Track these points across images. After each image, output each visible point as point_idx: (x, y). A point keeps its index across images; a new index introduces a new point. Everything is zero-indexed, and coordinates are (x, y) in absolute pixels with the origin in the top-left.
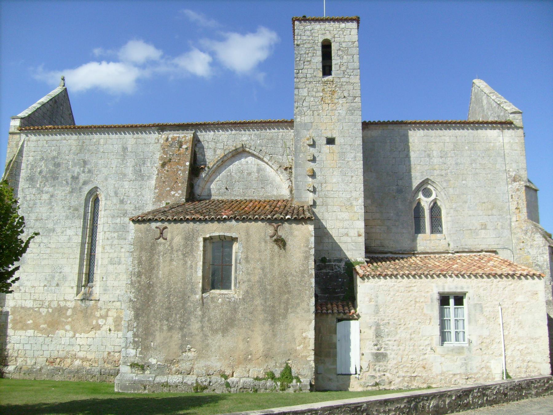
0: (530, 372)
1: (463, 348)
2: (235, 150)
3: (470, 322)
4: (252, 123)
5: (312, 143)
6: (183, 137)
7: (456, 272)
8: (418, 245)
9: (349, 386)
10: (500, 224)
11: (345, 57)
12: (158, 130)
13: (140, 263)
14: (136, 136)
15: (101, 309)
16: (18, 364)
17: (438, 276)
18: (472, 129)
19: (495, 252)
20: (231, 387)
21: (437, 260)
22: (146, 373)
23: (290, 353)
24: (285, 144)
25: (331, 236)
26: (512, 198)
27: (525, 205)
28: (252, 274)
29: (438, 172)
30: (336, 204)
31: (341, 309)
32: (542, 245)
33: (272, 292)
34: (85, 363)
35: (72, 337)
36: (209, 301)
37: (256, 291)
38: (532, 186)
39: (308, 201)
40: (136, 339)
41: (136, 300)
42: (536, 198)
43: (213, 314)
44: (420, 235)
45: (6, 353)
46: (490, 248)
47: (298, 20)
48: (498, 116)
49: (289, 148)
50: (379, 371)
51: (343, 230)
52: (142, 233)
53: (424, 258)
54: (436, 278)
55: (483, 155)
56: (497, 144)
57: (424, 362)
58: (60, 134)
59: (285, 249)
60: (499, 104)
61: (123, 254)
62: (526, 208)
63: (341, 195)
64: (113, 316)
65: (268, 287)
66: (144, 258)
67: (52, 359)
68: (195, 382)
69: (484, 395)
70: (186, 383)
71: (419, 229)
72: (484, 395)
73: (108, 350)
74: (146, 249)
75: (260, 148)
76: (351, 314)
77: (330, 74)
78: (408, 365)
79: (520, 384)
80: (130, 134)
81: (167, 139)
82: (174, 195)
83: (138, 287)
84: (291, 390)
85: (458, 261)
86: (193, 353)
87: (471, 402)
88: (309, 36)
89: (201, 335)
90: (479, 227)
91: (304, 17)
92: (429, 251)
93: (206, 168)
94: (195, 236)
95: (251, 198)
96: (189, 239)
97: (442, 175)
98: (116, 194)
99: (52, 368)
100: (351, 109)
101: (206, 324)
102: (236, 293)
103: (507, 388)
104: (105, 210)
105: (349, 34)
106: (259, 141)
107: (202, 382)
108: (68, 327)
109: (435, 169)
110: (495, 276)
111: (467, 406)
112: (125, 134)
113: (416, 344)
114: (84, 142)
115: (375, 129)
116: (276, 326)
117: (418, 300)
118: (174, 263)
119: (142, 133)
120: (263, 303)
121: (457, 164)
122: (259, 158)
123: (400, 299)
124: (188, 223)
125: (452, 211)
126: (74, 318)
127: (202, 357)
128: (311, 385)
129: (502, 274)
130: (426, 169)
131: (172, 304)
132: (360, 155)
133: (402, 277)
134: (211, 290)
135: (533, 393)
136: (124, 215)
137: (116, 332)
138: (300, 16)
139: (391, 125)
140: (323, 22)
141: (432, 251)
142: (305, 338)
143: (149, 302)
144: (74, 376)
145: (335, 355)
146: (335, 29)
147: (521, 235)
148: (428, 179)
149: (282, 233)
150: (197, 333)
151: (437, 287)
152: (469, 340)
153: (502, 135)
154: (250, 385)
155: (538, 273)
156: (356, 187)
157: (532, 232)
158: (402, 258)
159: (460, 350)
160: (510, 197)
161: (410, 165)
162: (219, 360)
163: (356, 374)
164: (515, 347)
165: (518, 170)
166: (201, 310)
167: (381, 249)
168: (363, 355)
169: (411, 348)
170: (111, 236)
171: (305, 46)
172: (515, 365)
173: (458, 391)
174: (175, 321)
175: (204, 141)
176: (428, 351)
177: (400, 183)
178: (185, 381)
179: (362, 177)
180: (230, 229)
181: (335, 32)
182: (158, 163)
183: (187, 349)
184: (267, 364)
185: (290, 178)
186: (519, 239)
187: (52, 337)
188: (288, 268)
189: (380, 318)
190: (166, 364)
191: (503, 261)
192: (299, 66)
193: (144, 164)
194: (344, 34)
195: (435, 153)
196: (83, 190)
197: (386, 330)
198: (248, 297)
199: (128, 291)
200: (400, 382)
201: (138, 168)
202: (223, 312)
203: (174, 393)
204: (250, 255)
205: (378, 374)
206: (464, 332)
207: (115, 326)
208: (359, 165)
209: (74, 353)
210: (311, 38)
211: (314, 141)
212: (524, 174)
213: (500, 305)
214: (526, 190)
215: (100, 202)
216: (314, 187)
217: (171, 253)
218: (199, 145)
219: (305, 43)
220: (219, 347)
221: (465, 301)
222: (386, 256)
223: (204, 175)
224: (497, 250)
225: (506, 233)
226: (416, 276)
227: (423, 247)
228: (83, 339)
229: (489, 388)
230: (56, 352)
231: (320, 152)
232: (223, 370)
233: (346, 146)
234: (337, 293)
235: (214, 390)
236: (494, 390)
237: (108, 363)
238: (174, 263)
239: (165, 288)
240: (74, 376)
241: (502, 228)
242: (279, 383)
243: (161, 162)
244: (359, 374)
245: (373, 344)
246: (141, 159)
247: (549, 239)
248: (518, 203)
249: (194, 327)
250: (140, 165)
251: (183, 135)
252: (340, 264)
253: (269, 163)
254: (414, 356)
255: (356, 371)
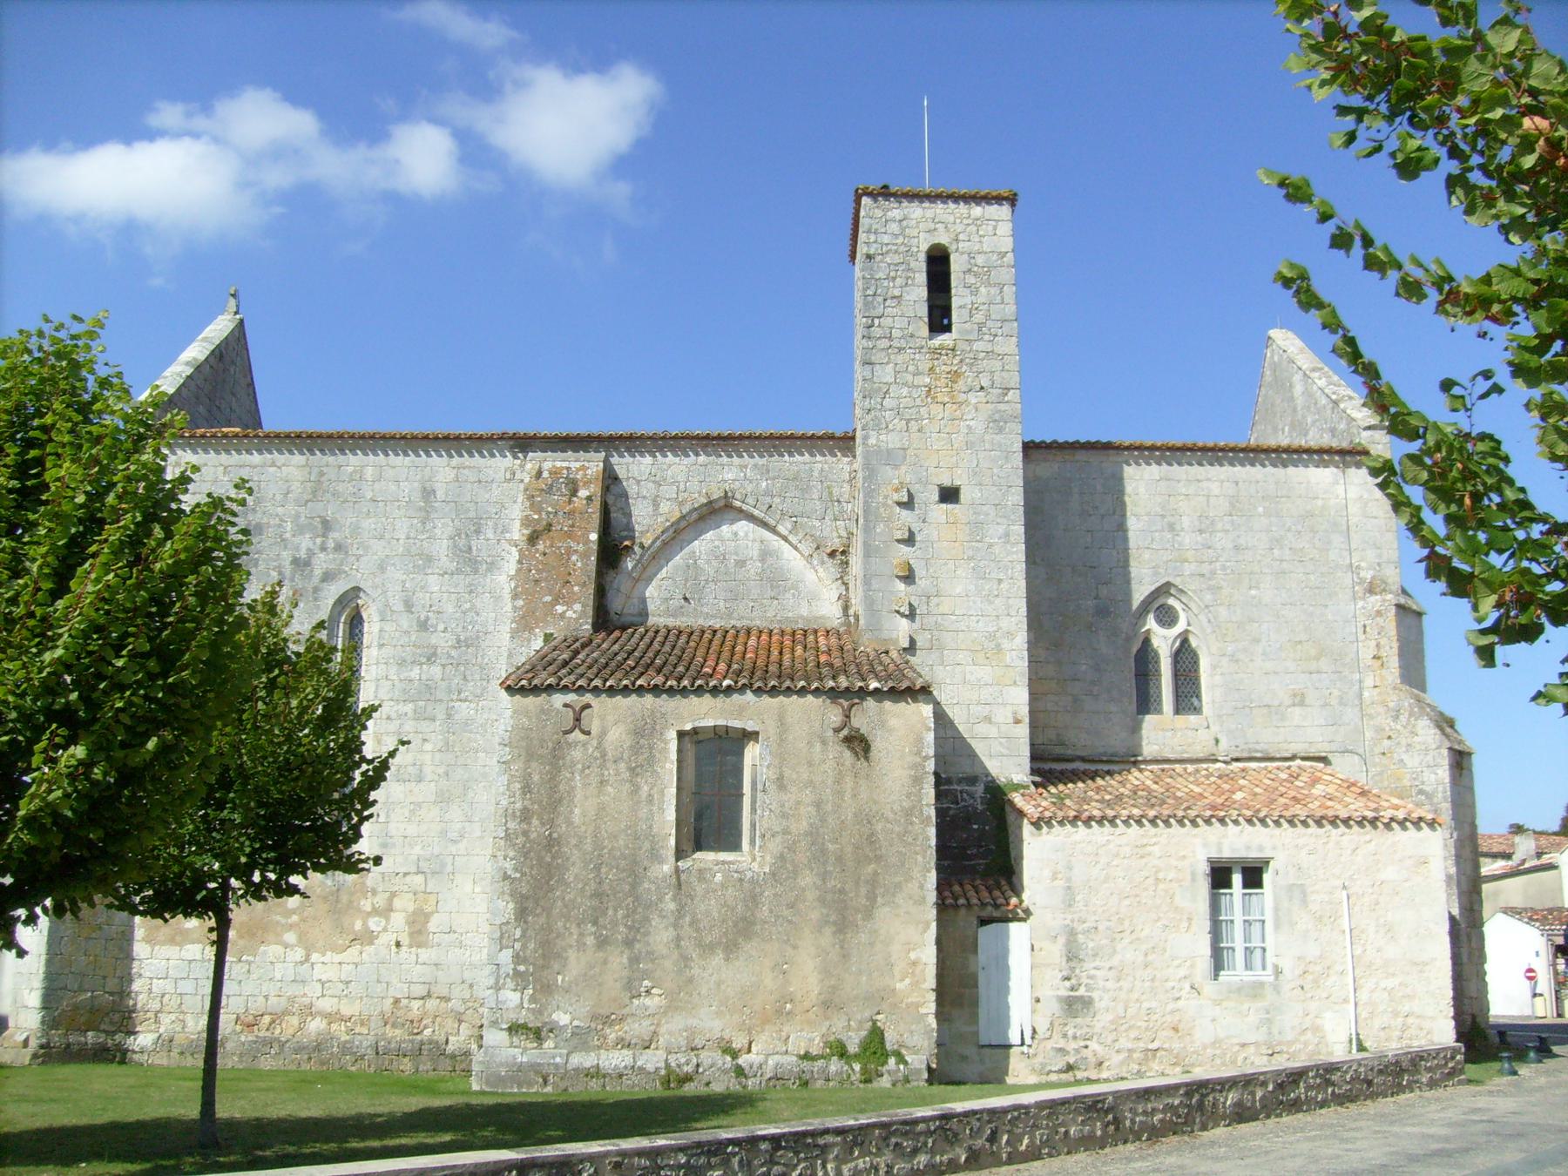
0: (1411, 1039)
1: (1262, 984)
2: (706, 505)
3: (1277, 926)
4: (749, 437)
5: (905, 499)
6: (578, 470)
7: (1248, 813)
8: (1144, 743)
9: (1006, 1073)
10: (1336, 693)
11: (983, 290)
12: (511, 449)
13: (526, 789)
14: (456, 460)
15: (374, 892)
16: (162, 1030)
17: (1208, 822)
18: (1275, 466)
19: (1324, 760)
20: (746, 1077)
21: (1191, 779)
22: (546, 1045)
23: (882, 997)
24: (830, 493)
25: (951, 723)
26: (1365, 632)
27: (1395, 650)
28: (793, 816)
29: (1193, 566)
30: (963, 647)
31: (985, 894)
32: (1434, 746)
33: (840, 859)
34: (334, 1027)
35: (302, 963)
36: (693, 879)
37: (802, 857)
38: (1410, 603)
39: (897, 639)
40: (522, 968)
41: (518, 875)
42: (1420, 633)
43: (703, 908)
44: (1148, 718)
45: (131, 1002)
46: (1313, 752)
47: (873, 195)
48: (1333, 431)
49: (838, 501)
50: (1075, 1038)
51: (979, 708)
52: (530, 719)
53: (1159, 773)
54: (1203, 827)
55: (1300, 528)
56: (1332, 502)
57: (1177, 1017)
58: (260, 452)
59: (867, 759)
60: (1336, 403)
61: (427, 758)
62: (1396, 658)
63: (973, 624)
64: (404, 911)
65: (830, 847)
66: (536, 778)
67: (251, 1017)
68: (662, 1065)
69: (1328, 1083)
70: (641, 1068)
71: (1145, 702)
72: (1328, 1083)
73: (392, 992)
74: (541, 756)
75: (768, 499)
76: (1011, 907)
77: (948, 329)
78: (1139, 1024)
79: (1397, 1062)
80: (442, 456)
81: (539, 474)
82: (562, 615)
83: (524, 846)
84: (885, 1082)
85: (1242, 782)
86: (657, 999)
87: (1303, 1096)
88: (896, 236)
89: (675, 956)
90: (1288, 701)
91: (885, 187)
92: (1172, 756)
93: (636, 548)
94: (658, 727)
95: (746, 623)
96: (644, 733)
97: (1203, 575)
98: (409, 606)
99: (250, 1038)
100: (997, 417)
101: (687, 931)
102: (754, 860)
103: (1372, 1070)
104: (381, 646)
105: (991, 233)
106: (764, 484)
107: (679, 1066)
108: (290, 937)
109: (1186, 561)
110: (1334, 822)
111: (1295, 1106)
112: (428, 455)
113: (1159, 975)
114: (322, 474)
115: (1046, 460)
116: (849, 936)
117: (1161, 875)
118: (610, 789)
119: (472, 456)
120: (819, 883)
121: (1236, 548)
122: (765, 525)
123: (1122, 874)
124: (657, 696)
125: (1225, 661)
126: (306, 914)
127: (677, 1008)
128: (929, 1069)
129: (1349, 818)
130: (1165, 558)
131: (606, 887)
132: (1019, 530)
133: (1125, 822)
134: (694, 852)
135: (1424, 1080)
136: (429, 660)
137: (414, 949)
138: (874, 186)
139: (1083, 452)
140: (931, 202)
141: (1178, 756)
142: (914, 963)
143: (551, 879)
144: (310, 1058)
145: (974, 1003)
146: (958, 221)
147: (1386, 722)
148: (1168, 584)
149: (860, 721)
150: (665, 951)
151: (1205, 845)
152: (1276, 967)
153: (1342, 482)
154: (791, 1071)
155: (1430, 816)
156: (1008, 607)
157: (1411, 715)
158: (1110, 773)
159: (1255, 991)
160: (1360, 630)
161: (1127, 549)
162: (719, 1014)
163: (1023, 1044)
164: (1377, 983)
165: (1379, 564)
166: (674, 899)
167: (1059, 750)
168: (1038, 1000)
169: (1147, 984)
170: (397, 711)
171: (888, 260)
172: (1377, 1023)
173: (1278, 1073)
174: (615, 923)
175: (628, 478)
176: (1183, 993)
177: (1104, 591)
178: (639, 1063)
179: (1023, 584)
180: (741, 711)
181: (959, 228)
182: (518, 533)
183: (642, 989)
184: (828, 1023)
185: (841, 578)
186: (1379, 730)
187: (249, 963)
188: (875, 802)
189: (1076, 916)
190: (593, 1025)
191: (1346, 785)
192: (874, 308)
193: (478, 532)
194: (981, 233)
195: (1186, 522)
196: (322, 594)
197: (1091, 945)
198: (782, 870)
199: (499, 854)
200: (1122, 1063)
201: (462, 543)
202: (725, 905)
203: (615, 1091)
204: (787, 772)
205: (1072, 1045)
206: (1264, 950)
207: (411, 935)
208: (1016, 552)
209: (306, 1001)
210: (900, 240)
211: (910, 496)
212: (1392, 576)
213: (1344, 887)
214: (1397, 614)
215: (366, 624)
216: (910, 604)
217: (602, 766)
218: (614, 489)
219: (887, 252)
220: (719, 984)
221: (1267, 878)
222: (1070, 766)
223: (630, 565)
224: (1330, 756)
225: (1351, 714)
226: (1158, 821)
227: (1156, 747)
228: (328, 966)
229: (1338, 1069)
230: (261, 999)
231: (924, 521)
232: (727, 1037)
233: (985, 508)
234: (971, 858)
235: (708, 1084)
236: (1346, 1072)
237: (394, 1026)
238: (610, 789)
239: (588, 847)
240: (310, 1058)
241: (1341, 703)
242: (857, 1067)
243: (526, 532)
244: (1030, 1046)
245: (1060, 976)
246: (472, 519)
247: (1448, 730)
248: (1378, 645)
249: (658, 939)
250: (467, 535)
251: (578, 465)
252: (973, 789)
253: (791, 538)
254: (1154, 1004)
255: (1023, 1039)
